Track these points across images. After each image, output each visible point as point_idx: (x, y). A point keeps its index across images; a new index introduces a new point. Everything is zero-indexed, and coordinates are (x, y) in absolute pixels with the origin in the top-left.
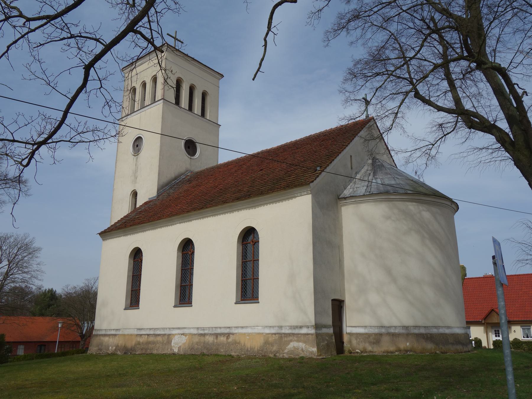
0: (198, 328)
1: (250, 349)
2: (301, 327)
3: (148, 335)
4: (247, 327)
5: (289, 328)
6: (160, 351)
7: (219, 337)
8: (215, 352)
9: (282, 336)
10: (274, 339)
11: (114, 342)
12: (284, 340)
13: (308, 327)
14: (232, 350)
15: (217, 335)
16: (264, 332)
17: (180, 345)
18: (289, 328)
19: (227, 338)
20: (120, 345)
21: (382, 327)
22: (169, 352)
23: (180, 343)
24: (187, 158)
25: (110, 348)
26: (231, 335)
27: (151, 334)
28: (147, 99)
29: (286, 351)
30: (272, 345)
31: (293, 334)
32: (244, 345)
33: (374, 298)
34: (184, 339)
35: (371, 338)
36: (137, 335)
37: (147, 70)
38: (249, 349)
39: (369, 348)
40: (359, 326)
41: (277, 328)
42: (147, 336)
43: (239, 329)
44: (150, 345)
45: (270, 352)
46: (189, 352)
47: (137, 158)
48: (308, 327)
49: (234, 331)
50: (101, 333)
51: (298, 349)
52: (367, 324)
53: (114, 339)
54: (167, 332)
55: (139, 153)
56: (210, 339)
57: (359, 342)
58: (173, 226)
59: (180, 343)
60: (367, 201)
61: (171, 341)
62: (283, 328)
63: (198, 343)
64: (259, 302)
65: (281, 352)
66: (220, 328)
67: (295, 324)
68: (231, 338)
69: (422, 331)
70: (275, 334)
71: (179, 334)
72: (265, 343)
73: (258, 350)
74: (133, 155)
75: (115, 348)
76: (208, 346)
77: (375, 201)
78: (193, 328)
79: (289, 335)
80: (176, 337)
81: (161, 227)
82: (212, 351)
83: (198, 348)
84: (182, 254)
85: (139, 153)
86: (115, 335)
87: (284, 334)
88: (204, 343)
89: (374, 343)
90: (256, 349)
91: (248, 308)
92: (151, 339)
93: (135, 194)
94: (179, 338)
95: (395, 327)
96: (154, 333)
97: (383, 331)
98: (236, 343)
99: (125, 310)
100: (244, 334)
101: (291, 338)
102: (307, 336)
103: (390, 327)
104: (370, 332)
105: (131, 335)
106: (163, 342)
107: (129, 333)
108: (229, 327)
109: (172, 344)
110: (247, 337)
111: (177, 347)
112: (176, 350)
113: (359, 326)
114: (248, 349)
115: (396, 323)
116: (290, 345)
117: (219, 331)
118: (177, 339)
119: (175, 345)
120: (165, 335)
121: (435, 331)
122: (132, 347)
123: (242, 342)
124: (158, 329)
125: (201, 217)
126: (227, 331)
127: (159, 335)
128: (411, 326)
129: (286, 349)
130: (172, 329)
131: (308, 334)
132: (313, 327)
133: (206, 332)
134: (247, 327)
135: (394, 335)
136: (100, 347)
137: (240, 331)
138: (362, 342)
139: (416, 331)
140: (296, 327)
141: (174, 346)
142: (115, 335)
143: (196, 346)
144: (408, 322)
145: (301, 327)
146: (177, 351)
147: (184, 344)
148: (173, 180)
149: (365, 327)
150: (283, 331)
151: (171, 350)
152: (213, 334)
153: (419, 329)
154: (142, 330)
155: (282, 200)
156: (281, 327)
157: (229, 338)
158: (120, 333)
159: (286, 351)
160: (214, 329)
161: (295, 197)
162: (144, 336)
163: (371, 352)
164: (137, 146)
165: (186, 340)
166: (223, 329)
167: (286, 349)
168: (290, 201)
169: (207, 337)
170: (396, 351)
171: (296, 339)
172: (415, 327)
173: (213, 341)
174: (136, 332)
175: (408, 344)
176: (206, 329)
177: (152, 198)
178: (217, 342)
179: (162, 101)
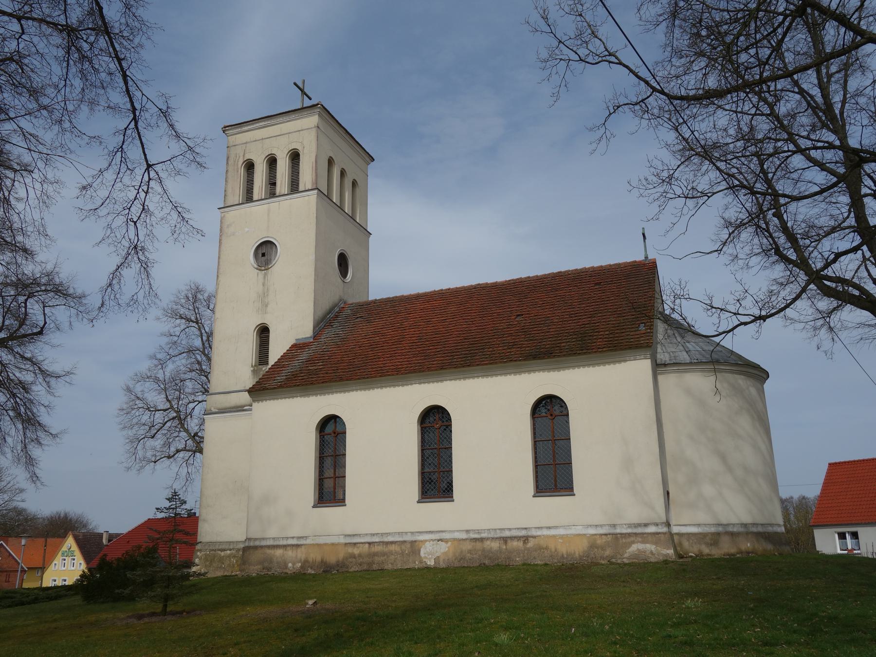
0: (468, 531)
1: (567, 555)
2: (646, 525)
3: (370, 543)
4: (556, 527)
5: (627, 526)
6: (399, 566)
7: (509, 541)
8: (506, 561)
9: (617, 537)
10: (604, 541)
11: (296, 556)
12: (621, 541)
13: (657, 525)
14: (535, 558)
15: (505, 540)
16: (586, 533)
17: (438, 554)
18: (627, 526)
19: (524, 542)
20: (310, 560)
21: (719, 525)
22: (417, 565)
23: (437, 552)
24: (340, 280)
25: (290, 565)
26: (530, 539)
27: (377, 542)
28: (281, 183)
29: (626, 555)
30: (603, 548)
31: (636, 534)
32: (556, 551)
33: (708, 490)
34: (443, 548)
35: (707, 538)
36: (346, 544)
37: (277, 137)
38: (565, 556)
39: (706, 550)
40: (690, 525)
41: (607, 527)
42: (367, 545)
43: (544, 530)
44: (376, 557)
45: (601, 557)
46: (457, 564)
47: (265, 274)
48: (657, 525)
49: (534, 533)
50: (264, 543)
51: (645, 552)
52: (701, 521)
53: (297, 552)
54: (409, 538)
55: (270, 266)
56: (495, 545)
57: (692, 543)
58: (406, 387)
59: (437, 552)
60: (693, 371)
61: (419, 551)
62: (618, 527)
63: (470, 550)
64: (453, 501)
65: (619, 556)
66: (510, 529)
67: (636, 521)
68: (532, 542)
69: (760, 529)
70: (606, 535)
71: (433, 540)
72: (591, 547)
73: (580, 556)
74: (257, 269)
75: (300, 564)
76: (491, 555)
77: (703, 371)
78: (457, 531)
79: (629, 535)
80: (427, 544)
81: (382, 387)
82: (500, 560)
83: (473, 558)
84: (422, 428)
85: (270, 266)
86: (298, 546)
87: (621, 534)
88: (484, 550)
89: (711, 545)
90: (577, 555)
91: (330, 513)
92: (377, 549)
93: (263, 332)
94: (435, 546)
95: (734, 525)
96: (382, 540)
97: (720, 529)
98: (540, 548)
99: (420, 504)
100: (554, 536)
101: (632, 539)
102: (657, 536)
103: (728, 525)
104: (705, 532)
105: (338, 544)
106: (402, 552)
107: (333, 541)
108: (526, 528)
109: (422, 554)
110: (560, 540)
111: (432, 558)
112: (431, 563)
113: (690, 525)
114: (563, 555)
115: (734, 520)
116: (632, 548)
117: (507, 534)
118: (431, 548)
119: (429, 555)
120: (405, 542)
121: (770, 529)
122: (338, 561)
123: (552, 546)
124: (388, 534)
125: (462, 376)
126: (523, 533)
127: (392, 543)
128: (749, 524)
129: (626, 553)
130: (417, 534)
131: (658, 533)
132: (664, 525)
133: (484, 535)
134: (556, 527)
135: (732, 534)
136: (266, 564)
137: (546, 532)
138: (696, 543)
139: (754, 530)
140: (639, 525)
141: (425, 557)
142: (298, 546)
143: (469, 555)
144: (747, 519)
145: (646, 525)
146: (433, 563)
147: (445, 553)
148: (328, 314)
149: (699, 525)
150: (618, 531)
151: (421, 562)
152: (497, 538)
153: (757, 527)
154: (355, 537)
155: (604, 364)
156: (614, 526)
157: (528, 542)
158: (308, 541)
159: (626, 555)
160: (498, 531)
161: (625, 361)
162: (361, 545)
163: (708, 555)
164: (263, 255)
165: (448, 548)
166: (514, 531)
167: (626, 553)
168: (617, 365)
169: (487, 543)
170: (738, 553)
171: (640, 539)
172: (754, 524)
173: (500, 547)
174: (342, 540)
175: (749, 545)
176: (483, 531)
177: (303, 338)
178: (506, 549)
179: (316, 191)
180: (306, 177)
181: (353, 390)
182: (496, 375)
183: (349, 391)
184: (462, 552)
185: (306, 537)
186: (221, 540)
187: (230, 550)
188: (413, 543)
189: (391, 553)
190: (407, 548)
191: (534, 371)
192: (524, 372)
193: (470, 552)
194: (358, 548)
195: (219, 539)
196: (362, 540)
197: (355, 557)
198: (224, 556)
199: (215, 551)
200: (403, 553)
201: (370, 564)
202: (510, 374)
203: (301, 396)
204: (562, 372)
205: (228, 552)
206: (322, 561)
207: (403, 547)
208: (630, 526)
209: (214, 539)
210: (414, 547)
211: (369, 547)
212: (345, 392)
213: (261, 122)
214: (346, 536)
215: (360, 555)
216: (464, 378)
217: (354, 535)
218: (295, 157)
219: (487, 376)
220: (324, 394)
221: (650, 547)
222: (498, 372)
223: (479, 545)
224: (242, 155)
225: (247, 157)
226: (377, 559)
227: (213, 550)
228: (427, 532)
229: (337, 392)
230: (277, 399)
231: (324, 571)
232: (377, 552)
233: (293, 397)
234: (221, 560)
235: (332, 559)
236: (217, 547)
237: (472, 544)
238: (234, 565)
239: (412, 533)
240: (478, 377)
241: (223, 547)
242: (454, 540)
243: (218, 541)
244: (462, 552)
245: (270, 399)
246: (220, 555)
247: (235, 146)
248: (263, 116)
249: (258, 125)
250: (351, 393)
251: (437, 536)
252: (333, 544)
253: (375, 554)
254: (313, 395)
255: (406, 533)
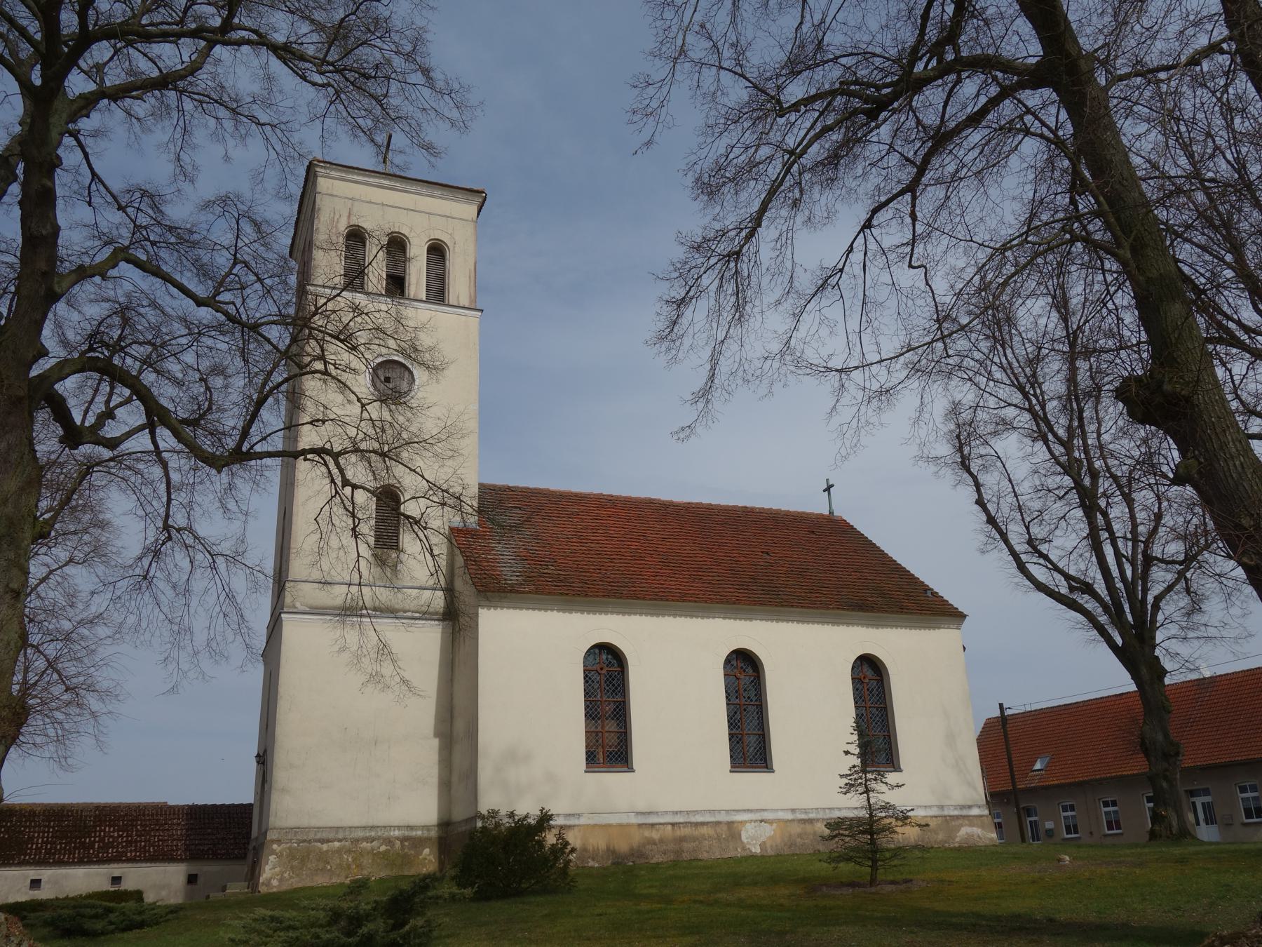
0: (793, 810)
2: (970, 807)
3: (673, 825)
9: (948, 819)
17: (763, 839)
20: (591, 848)
22: (739, 853)
29: (957, 840)
34: (767, 831)
36: (640, 825)
41: (935, 809)
42: (669, 827)
46: (787, 851)
61: (740, 835)
66: (840, 809)
67: (962, 803)
70: (936, 817)
78: (782, 810)
79: (958, 817)
91: (613, 781)
101: (960, 821)
105: (628, 825)
109: (744, 838)
120: (718, 823)
122: (632, 849)
124: (696, 812)
127: (703, 824)
133: (812, 816)
141: (748, 843)
143: (799, 840)
145: (970, 807)
147: (771, 838)
150: (946, 813)
151: (744, 849)
156: (942, 807)
158: (583, 821)
159: (957, 840)
174: (634, 820)
180: (459, 285)
181: (635, 614)
182: (813, 622)
183: (630, 614)
184: (790, 836)
185: (579, 815)
186: (320, 824)
187: (340, 841)
188: (730, 824)
189: (703, 837)
190: (723, 830)
191: (853, 624)
192: (843, 624)
193: (800, 835)
194: (658, 830)
195: (315, 823)
196: (662, 820)
197: (655, 844)
198: (327, 851)
199: (309, 842)
200: (719, 838)
201: (679, 852)
202: (828, 623)
203: (559, 610)
204: (880, 630)
205: (337, 844)
206: (608, 849)
207: (718, 830)
208: (956, 807)
209: (305, 822)
210: (732, 829)
211: (673, 829)
212: (624, 614)
213: (340, 171)
214: (638, 813)
215: (661, 841)
216: (777, 621)
217: (650, 813)
218: (437, 251)
219: (803, 622)
220: (594, 612)
221: (976, 831)
222: (816, 620)
223: (809, 828)
224: (345, 215)
225: (354, 221)
226: (685, 845)
227: (305, 841)
228: (744, 811)
229: (612, 613)
230: (521, 608)
231: (613, 864)
232: (685, 836)
233: (546, 610)
234: (323, 857)
235: (623, 846)
236: (311, 836)
237: (802, 826)
238: (349, 866)
239: (727, 811)
240: (793, 621)
241: (324, 835)
242: (779, 821)
243: (312, 825)
244: (790, 836)
245: (508, 608)
246: (320, 849)
247: (332, 195)
248: (440, 182)
249: (377, 180)
250: (633, 617)
251: (758, 816)
252: (620, 825)
253: (682, 839)
254: (577, 611)
255: (719, 811)
